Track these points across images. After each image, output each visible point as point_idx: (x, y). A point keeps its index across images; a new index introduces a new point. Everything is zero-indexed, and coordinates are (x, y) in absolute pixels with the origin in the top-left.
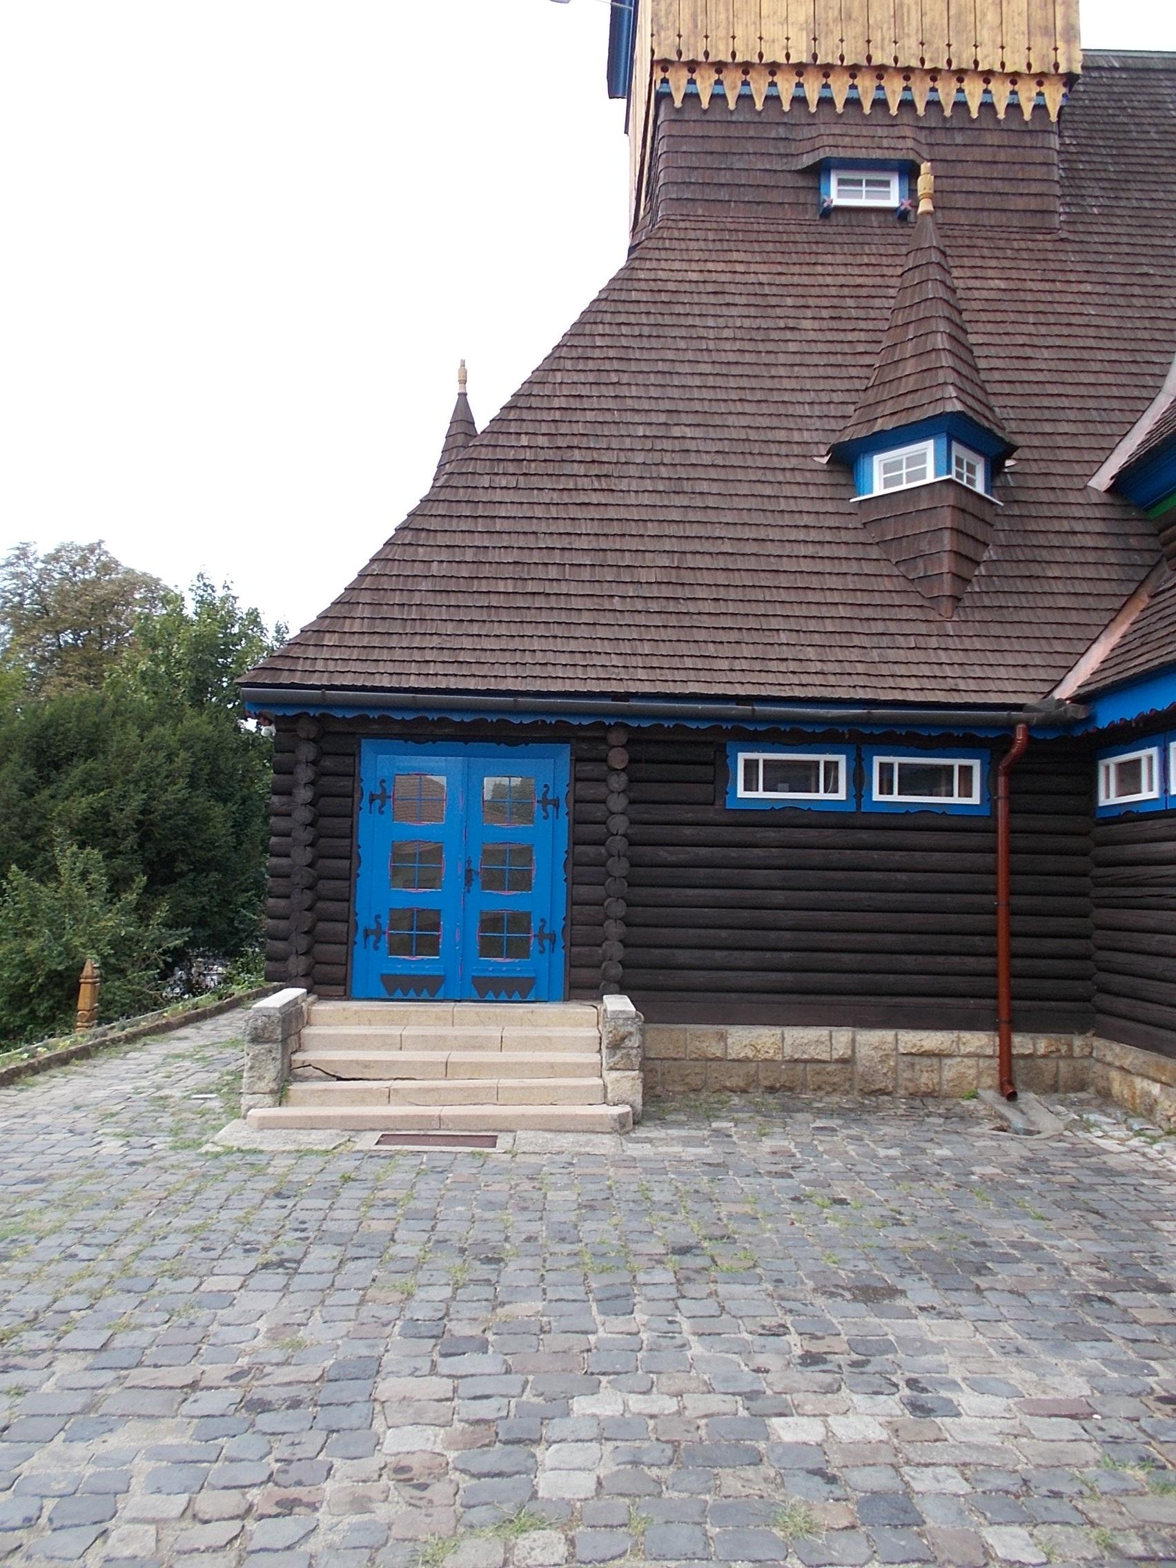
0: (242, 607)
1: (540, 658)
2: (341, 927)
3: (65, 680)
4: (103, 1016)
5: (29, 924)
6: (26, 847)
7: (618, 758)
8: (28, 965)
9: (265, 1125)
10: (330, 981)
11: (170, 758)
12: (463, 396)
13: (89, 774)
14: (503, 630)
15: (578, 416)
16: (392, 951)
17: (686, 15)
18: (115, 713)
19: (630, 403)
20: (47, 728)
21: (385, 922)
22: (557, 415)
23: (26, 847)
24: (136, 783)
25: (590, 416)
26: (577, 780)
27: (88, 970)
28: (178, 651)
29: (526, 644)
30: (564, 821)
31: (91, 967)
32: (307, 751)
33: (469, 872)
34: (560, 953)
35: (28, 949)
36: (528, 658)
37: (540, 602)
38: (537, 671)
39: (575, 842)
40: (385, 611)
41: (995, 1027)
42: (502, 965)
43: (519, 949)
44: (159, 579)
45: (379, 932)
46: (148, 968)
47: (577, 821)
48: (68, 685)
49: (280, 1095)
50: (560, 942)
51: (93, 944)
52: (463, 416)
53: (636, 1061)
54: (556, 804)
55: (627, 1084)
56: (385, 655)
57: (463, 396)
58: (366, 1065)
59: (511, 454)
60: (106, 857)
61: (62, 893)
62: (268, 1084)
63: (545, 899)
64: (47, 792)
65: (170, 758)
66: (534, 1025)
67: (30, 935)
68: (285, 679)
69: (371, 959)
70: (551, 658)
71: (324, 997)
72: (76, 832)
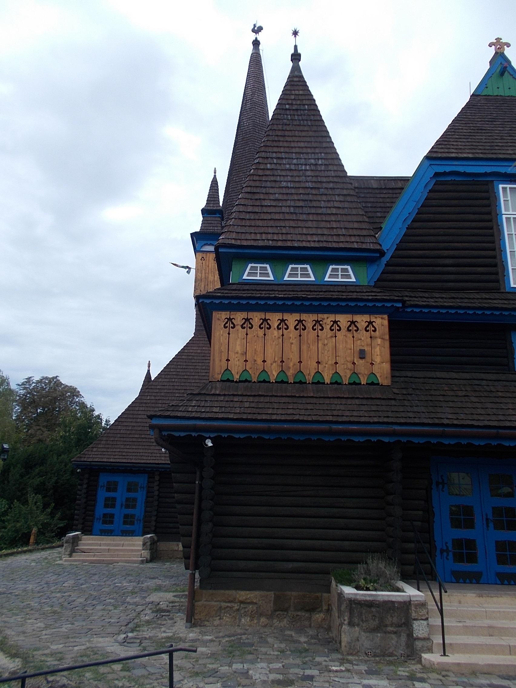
0: (96, 413)
1: (141, 454)
2: (91, 518)
3: (38, 427)
4: (37, 543)
5: (18, 518)
6: (20, 494)
7: (157, 478)
8: (17, 531)
9: (66, 561)
10: (88, 531)
11: (65, 466)
14: (134, 447)
15: (162, 391)
16: (103, 524)
17: (203, 286)
18: (50, 451)
19: (176, 387)
20: (30, 455)
21: (102, 516)
22: (158, 391)
24: (54, 474)
25: (166, 391)
26: (149, 482)
27: (33, 531)
28: (73, 429)
29: (139, 451)
30: (145, 492)
31: (35, 530)
32: (87, 476)
34: (142, 524)
35: (17, 526)
36: (138, 454)
37: (144, 440)
38: (140, 457)
39: (147, 497)
40: (108, 442)
42: (128, 527)
43: (132, 523)
44: (76, 388)
45: (447, 551)
46: (53, 533)
47: (148, 492)
48: (40, 429)
49: (70, 555)
50: (142, 521)
51: (36, 524)
52: (148, 374)
53: (149, 548)
55: (146, 553)
56: (106, 453)
58: (91, 549)
59: (145, 401)
60: (43, 497)
61: (29, 509)
62: (68, 553)
63: (139, 511)
64: (27, 477)
65: (65, 466)
66: (132, 541)
67: (18, 521)
68: (82, 460)
69: (98, 525)
70: (144, 454)
71: (85, 535)
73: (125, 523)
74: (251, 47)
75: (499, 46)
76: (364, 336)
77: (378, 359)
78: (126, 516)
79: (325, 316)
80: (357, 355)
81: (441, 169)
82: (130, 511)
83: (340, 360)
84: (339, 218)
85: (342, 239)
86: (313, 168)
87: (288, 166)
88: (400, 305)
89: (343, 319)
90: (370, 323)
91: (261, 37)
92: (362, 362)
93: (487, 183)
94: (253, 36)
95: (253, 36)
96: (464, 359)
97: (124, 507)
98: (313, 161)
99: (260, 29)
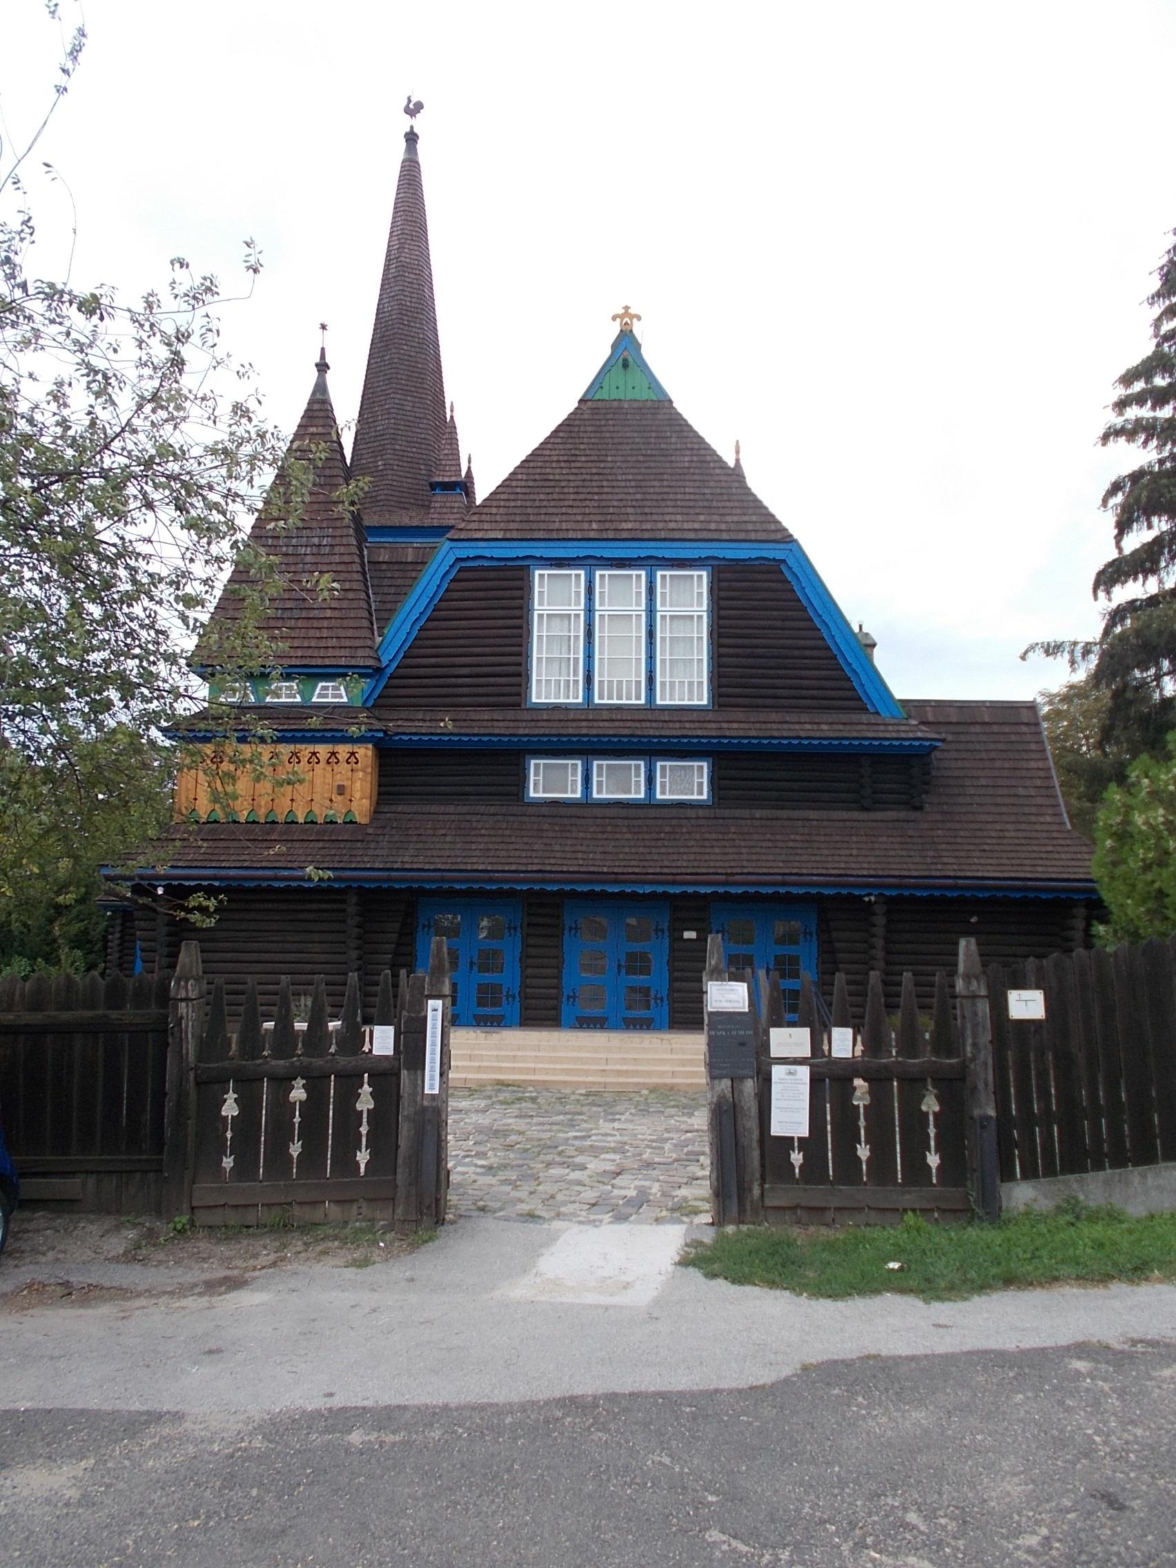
12: (321, 387)
13: (80, 912)
23: (48, 949)
32: (119, 921)
33: (619, 966)
34: (517, 1005)
41: (770, 1065)
42: (489, 1010)
43: (496, 1003)
54: (514, 997)
57: (321, 387)
72: (72, 941)
73: (479, 1005)
74: (404, 145)
75: (626, 318)
76: (344, 768)
77: (357, 795)
78: (482, 988)
79: (303, 746)
80: (335, 790)
81: (463, 554)
82: (640, 980)
83: (317, 797)
84: (333, 623)
85: (330, 653)
86: (315, 550)
87: (284, 549)
88: (381, 735)
89: (323, 750)
90: (353, 754)
91: (420, 124)
92: (339, 798)
93: (522, 568)
94: (405, 122)
95: (405, 122)
96: (467, 789)
97: (475, 968)
98: (316, 541)
99: (419, 106)
